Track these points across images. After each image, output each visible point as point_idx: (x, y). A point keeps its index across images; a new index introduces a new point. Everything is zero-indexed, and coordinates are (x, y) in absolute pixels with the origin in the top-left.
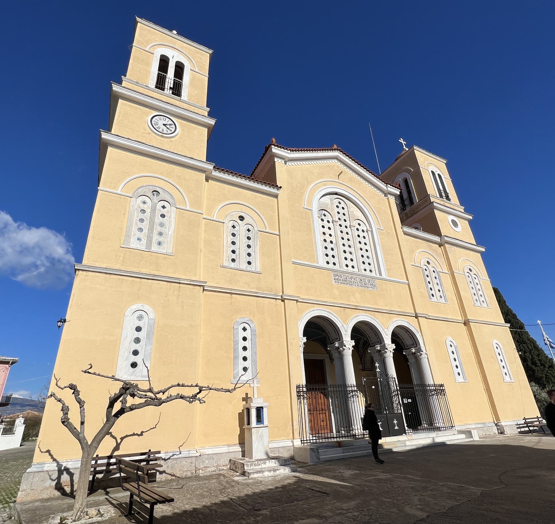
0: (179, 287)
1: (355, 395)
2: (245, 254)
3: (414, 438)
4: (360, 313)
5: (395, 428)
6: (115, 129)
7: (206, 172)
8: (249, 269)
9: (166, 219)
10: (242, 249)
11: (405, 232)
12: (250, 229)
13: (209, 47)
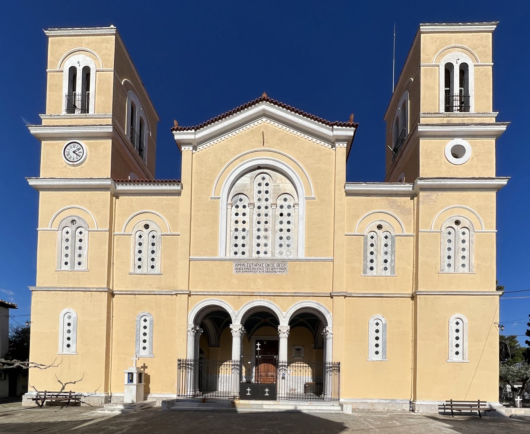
0: (92, 294)
2: (150, 260)
3: (281, 404)
4: (256, 298)
5: (265, 395)
7: (110, 188)
8: (152, 273)
10: (146, 255)
11: (349, 192)
12: (155, 236)
13: (105, 24)
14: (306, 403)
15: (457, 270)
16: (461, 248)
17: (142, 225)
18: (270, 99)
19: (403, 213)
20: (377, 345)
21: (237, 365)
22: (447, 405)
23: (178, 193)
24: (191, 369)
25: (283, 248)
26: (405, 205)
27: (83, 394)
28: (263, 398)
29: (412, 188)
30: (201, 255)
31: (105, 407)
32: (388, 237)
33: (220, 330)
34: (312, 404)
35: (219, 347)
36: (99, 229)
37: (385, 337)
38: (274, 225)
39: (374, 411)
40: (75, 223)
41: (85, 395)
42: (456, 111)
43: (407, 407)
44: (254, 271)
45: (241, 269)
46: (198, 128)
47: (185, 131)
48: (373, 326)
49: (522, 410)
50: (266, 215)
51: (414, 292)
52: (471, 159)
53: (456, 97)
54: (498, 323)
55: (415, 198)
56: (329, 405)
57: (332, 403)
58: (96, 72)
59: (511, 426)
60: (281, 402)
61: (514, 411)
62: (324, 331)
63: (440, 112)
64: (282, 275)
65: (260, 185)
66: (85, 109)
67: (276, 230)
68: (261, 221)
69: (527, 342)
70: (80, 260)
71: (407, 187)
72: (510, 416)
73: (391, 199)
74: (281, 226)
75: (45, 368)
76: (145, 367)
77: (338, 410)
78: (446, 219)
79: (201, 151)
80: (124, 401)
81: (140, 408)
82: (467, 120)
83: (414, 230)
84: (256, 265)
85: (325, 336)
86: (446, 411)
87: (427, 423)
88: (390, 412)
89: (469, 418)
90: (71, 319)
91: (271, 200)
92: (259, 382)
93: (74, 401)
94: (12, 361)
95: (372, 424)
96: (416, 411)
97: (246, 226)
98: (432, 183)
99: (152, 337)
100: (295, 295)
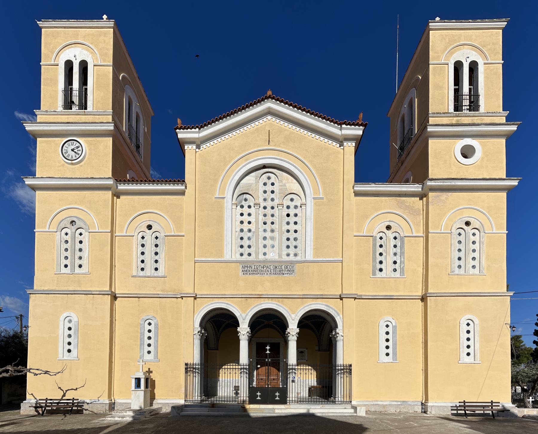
0: (93, 297)
1: (243, 372)
2: (153, 262)
3: (292, 407)
5: (276, 399)
6: (38, 172)
8: (156, 275)
9: (83, 245)
10: (149, 257)
14: (317, 406)
15: (467, 272)
16: (472, 250)
17: (145, 225)
18: (276, 97)
19: (413, 214)
20: (387, 347)
21: (246, 369)
22: (460, 406)
23: (182, 193)
24: (198, 373)
25: (290, 249)
26: (414, 205)
27: (85, 401)
28: (274, 402)
29: (422, 189)
30: (206, 256)
31: (113, 413)
32: (397, 238)
33: (220, 332)
34: (324, 408)
35: (218, 350)
36: (100, 231)
37: (396, 339)
38: (281, 226)
39: (386, 413)
40: (75, 224)
41: (88, 402)
42: (466, 111)
43: (419, 409)
44: (262, 273)
45: (248, 271)
46: (202, 127)
47: (189, 130)
48: (383, 328)
49: (534, 410)
50: (273, 216)
51: (423, 294)
52: (481, 158)
53: (466, 96)
54: (510, 324)
55: (425, 199)
56: (342, 408)
57: (344, 406)
58: (94, 67)
59: (526, 426)
60: (293, 406)
61: (526, 412)
62: (334, 333)
63: (449, 112)
64: (290, 277)
65: (265, 184)
66: (83, 106)
67: (283, 231)
68: (267, 222)
69: (535, 342)
70: (81, 262)
71: (416, 188)
72: (523, 417)
73: (400, 199)
74: (288, 227)
75: (55, 375)
76: (149, 372)
77: (351, 413)
78: (457, 220)
79: (204, 150)
80: (131, 408)
81: (149, 415)
82: (477, 119)
83: (423, 230)
84: (263, 267)
85: (335, 338)
86: (459, 412)
87: (443, 424)
88: (403, 414)
89: (482, 419)
90: (72, 323)
91: (277, 200)
92: (270, 386)
93: (76, 408)
94: (18, 368)
95: (391, 426)
96: (428, 413)
97: (252, 227)
98: (442, 183)
99: (157, 341)
100: (304, 297)
